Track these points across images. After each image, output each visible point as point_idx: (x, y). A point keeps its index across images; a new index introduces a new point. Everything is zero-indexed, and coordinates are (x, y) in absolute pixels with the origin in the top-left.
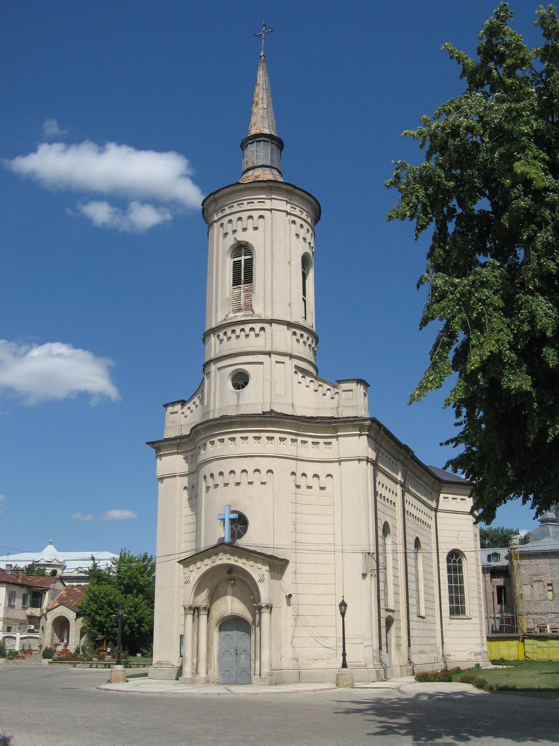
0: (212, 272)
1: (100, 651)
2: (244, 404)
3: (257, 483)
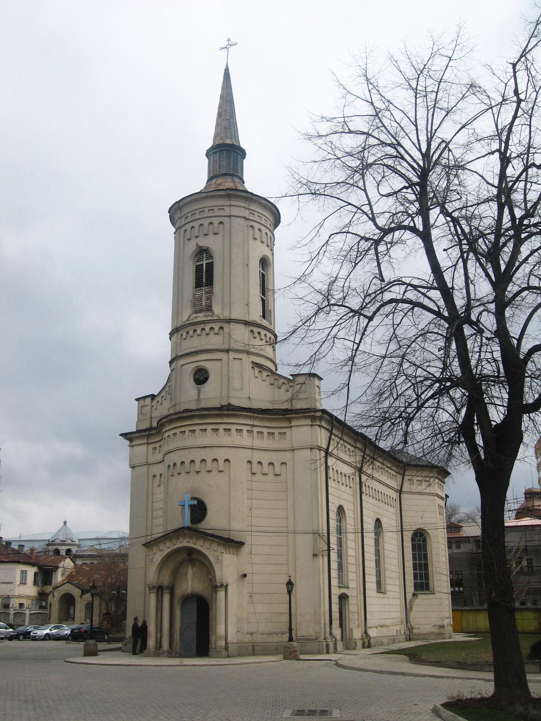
2: (204, 399)
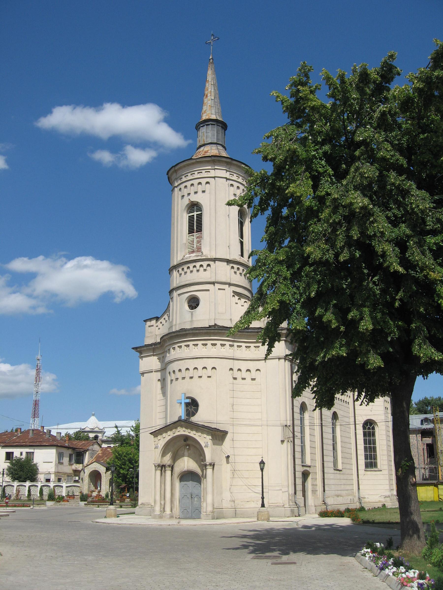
0: (174, 224)
1: (123, 496)
3: (205, 377)
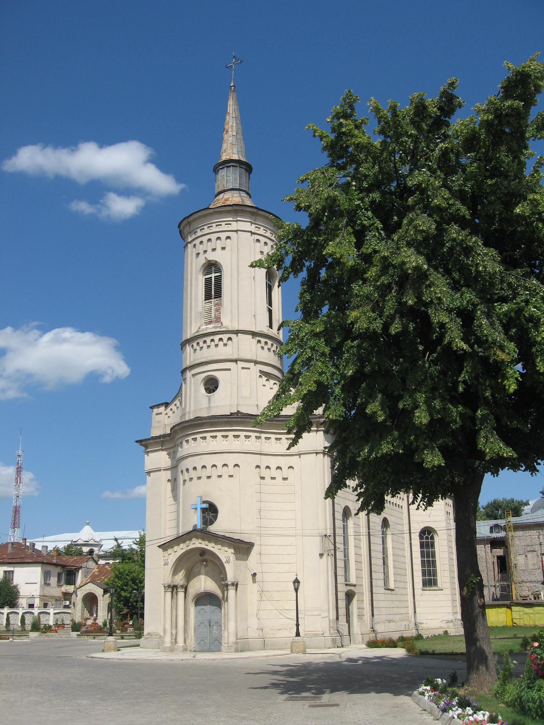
0: (187, 289)
1: (124, 624)
